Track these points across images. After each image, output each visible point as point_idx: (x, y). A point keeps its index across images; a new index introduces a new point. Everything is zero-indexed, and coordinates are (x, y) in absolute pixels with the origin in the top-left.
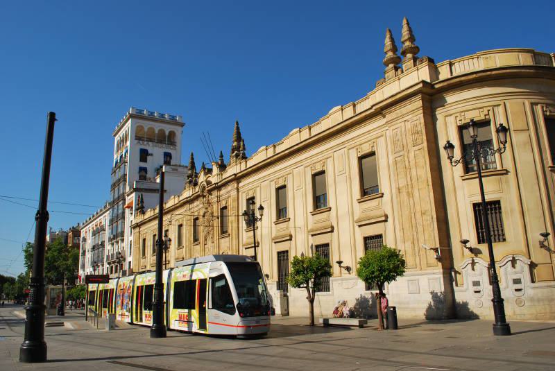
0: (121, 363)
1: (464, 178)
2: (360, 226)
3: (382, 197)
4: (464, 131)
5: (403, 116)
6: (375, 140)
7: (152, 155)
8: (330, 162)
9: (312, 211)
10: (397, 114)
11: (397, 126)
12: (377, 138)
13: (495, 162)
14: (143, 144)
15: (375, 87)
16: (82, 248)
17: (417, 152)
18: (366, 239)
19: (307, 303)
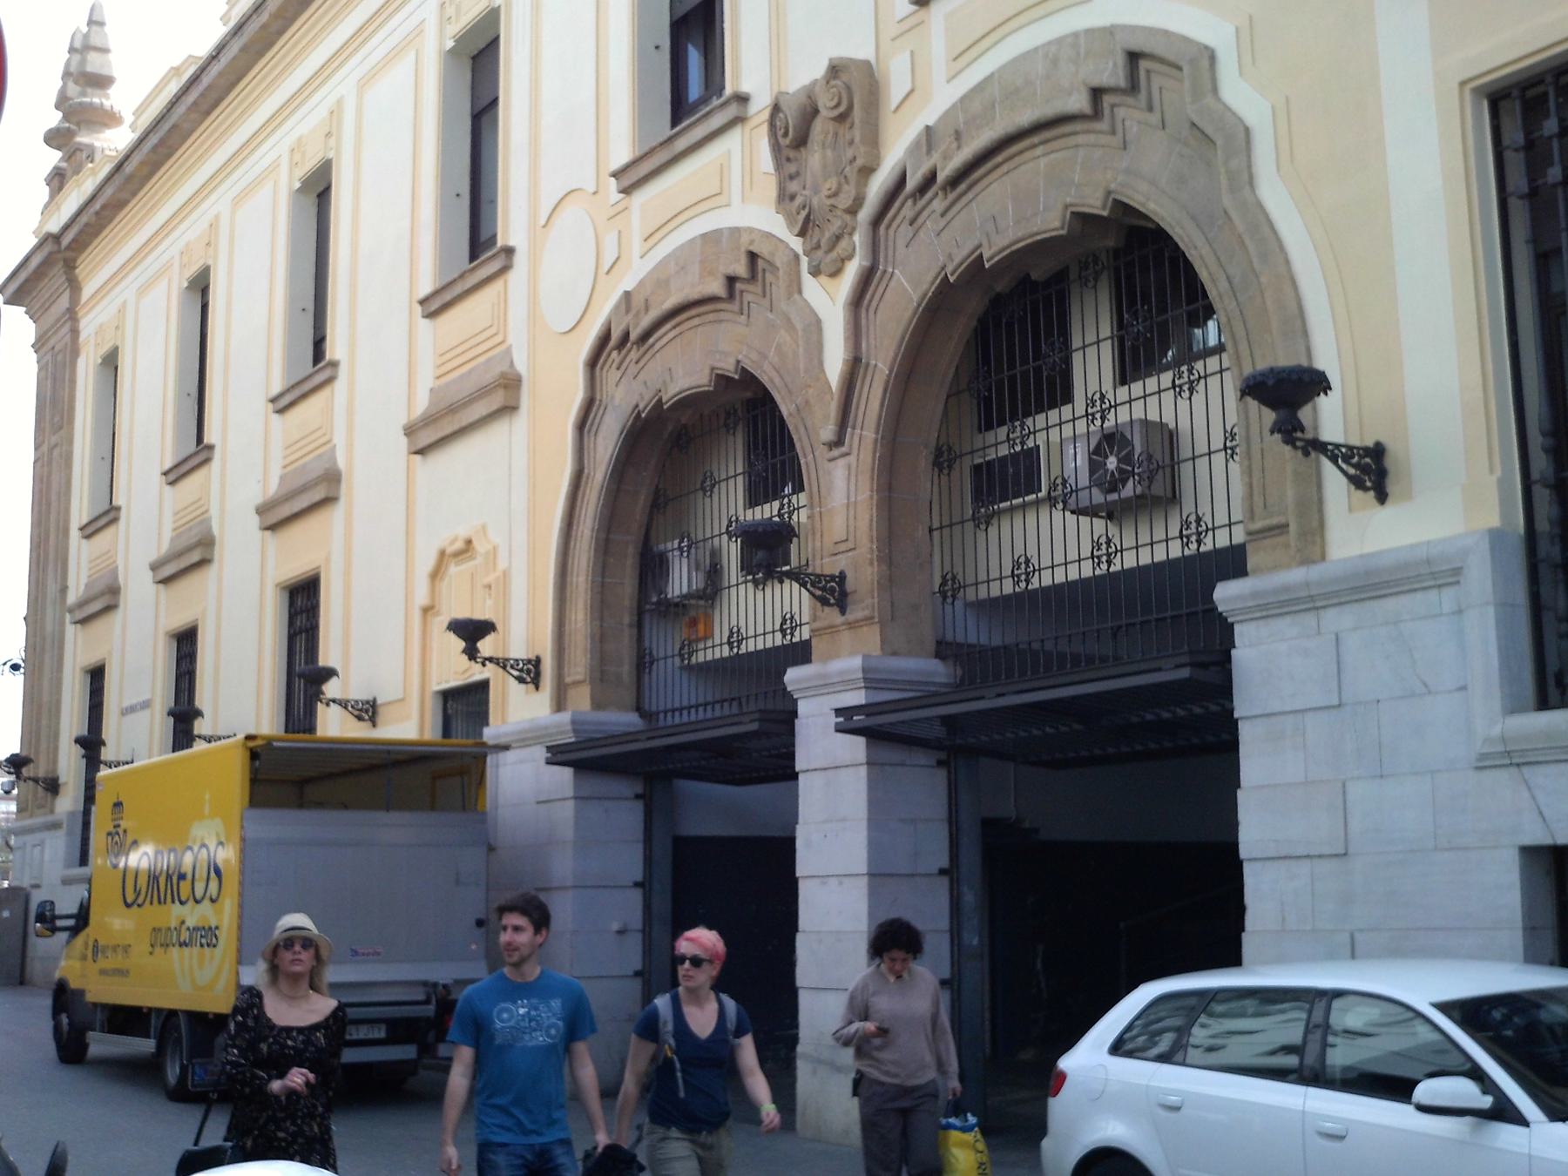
0: (957, 834)
4: (1116, 109)
7: (165, 952)
16: (1187, 287)
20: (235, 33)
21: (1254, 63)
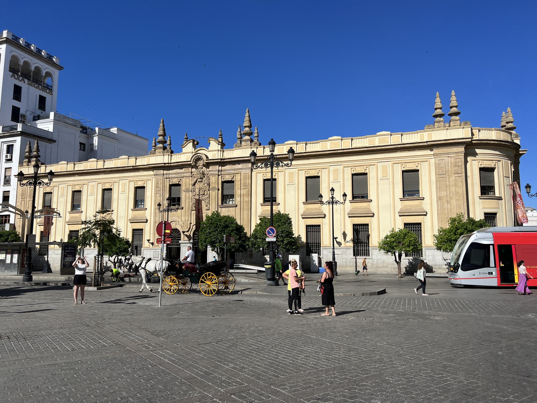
1: (351, 202)
2: (39, 225)
3: (236, 207)
5: (448, 153)
8: (116, 185)
9: (132, 208)
10: (444, 151)
11: (443, 158)
12: (421, 162)
14: (18, 79)
17: (457, 178)
18: (134, 230)
19: (396, 265)
20: (136, 205)
21: (242, 301)
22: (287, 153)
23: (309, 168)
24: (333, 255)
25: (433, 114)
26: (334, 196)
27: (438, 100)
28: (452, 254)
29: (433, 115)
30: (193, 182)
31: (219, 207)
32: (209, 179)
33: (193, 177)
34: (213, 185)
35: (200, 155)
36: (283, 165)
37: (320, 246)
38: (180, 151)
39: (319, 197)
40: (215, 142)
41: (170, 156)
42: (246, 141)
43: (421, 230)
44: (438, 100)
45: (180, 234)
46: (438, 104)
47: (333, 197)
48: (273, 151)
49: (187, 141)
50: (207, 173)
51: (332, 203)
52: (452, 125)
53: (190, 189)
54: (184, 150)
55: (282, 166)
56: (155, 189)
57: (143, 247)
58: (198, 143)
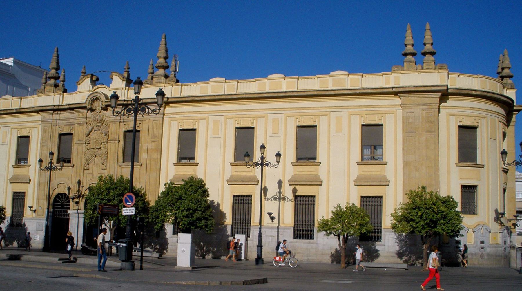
1: (294, 164)
6: (31, 129)
11: (413, 110)
13: (48, 142)
15: (390, 70)
17: (429, 138)
22: (155, 96)
23: (182, 118)
24: (259, 236)
25: (403, 52)
26: (264, 156)
27: (409, 34)
28: (27, 221)
29: (402, 53)
30: (88, 133)
31: (119, 167)
32: (108, 128)
33: (88, 124)
34: (113, 135)
35: (99, 95)
36: (150, 111)
37: (250, 225)
38: (74, 89)
39: (245, 156)
40: (118, 78)
41: (62, 96)
42: (159, 76)
43: (314, 204)
44: (409, 34)
45: (69, 202)
46: (409, 39)
47: (262, 157)
48: (138, 93)
49: (84, 76)
50: (106, 119)
51: (261, 165)
52: (425, 67)
53: (84, 140)
54: (80, 88)
55: (149, 113)
56: (42, 140)
57: (25, 216)
58: (98, 79)
